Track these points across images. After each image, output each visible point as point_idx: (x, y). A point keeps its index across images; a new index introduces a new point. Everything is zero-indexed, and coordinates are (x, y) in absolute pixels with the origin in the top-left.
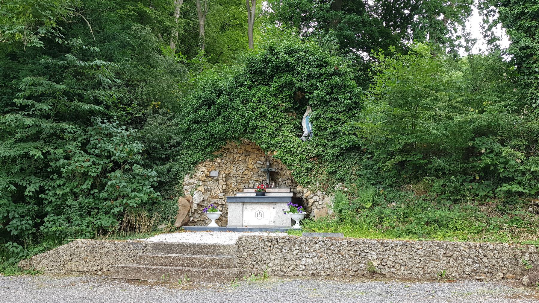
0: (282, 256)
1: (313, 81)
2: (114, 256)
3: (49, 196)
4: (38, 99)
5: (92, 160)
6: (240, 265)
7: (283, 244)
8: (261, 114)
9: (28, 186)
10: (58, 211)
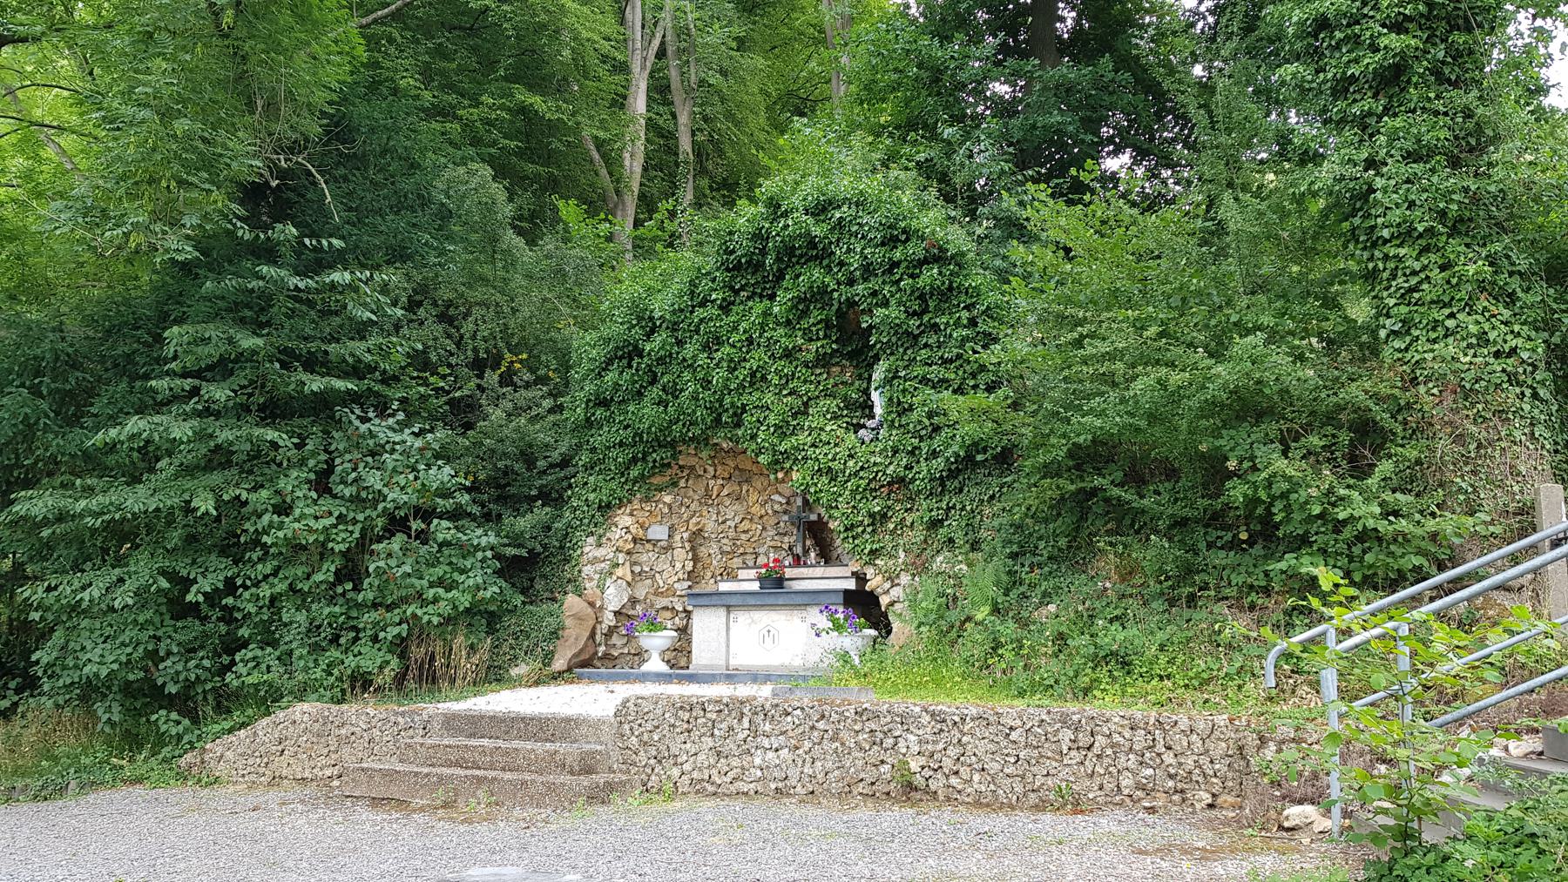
0: (711, 744)
1: (874, 284)
5: (336, 514)
7: (714, 716)
8: (753, 374)
9: (200, 578)
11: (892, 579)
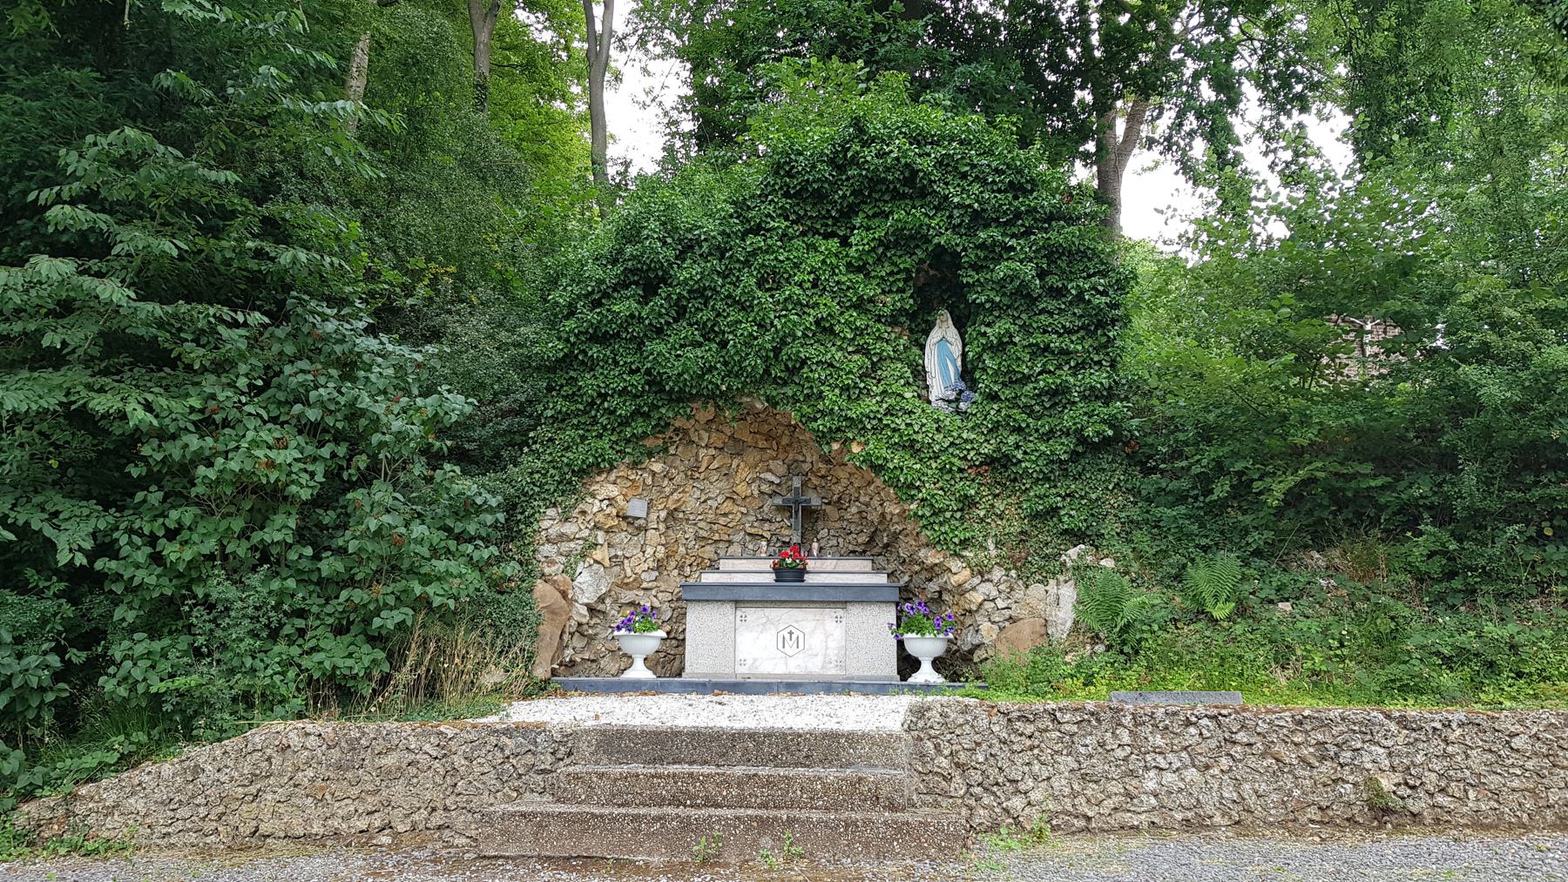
2: (438, 779)
3: (133, 564)
4: (131, 211)
6: (929, 799)
7: (1075, 728)
8: (817, 322)
10: (164, 616)
11: (981, 572)
